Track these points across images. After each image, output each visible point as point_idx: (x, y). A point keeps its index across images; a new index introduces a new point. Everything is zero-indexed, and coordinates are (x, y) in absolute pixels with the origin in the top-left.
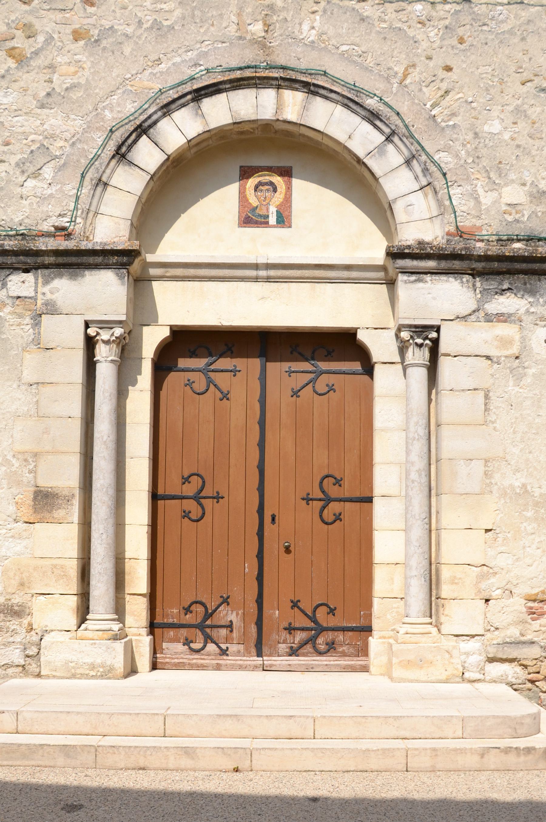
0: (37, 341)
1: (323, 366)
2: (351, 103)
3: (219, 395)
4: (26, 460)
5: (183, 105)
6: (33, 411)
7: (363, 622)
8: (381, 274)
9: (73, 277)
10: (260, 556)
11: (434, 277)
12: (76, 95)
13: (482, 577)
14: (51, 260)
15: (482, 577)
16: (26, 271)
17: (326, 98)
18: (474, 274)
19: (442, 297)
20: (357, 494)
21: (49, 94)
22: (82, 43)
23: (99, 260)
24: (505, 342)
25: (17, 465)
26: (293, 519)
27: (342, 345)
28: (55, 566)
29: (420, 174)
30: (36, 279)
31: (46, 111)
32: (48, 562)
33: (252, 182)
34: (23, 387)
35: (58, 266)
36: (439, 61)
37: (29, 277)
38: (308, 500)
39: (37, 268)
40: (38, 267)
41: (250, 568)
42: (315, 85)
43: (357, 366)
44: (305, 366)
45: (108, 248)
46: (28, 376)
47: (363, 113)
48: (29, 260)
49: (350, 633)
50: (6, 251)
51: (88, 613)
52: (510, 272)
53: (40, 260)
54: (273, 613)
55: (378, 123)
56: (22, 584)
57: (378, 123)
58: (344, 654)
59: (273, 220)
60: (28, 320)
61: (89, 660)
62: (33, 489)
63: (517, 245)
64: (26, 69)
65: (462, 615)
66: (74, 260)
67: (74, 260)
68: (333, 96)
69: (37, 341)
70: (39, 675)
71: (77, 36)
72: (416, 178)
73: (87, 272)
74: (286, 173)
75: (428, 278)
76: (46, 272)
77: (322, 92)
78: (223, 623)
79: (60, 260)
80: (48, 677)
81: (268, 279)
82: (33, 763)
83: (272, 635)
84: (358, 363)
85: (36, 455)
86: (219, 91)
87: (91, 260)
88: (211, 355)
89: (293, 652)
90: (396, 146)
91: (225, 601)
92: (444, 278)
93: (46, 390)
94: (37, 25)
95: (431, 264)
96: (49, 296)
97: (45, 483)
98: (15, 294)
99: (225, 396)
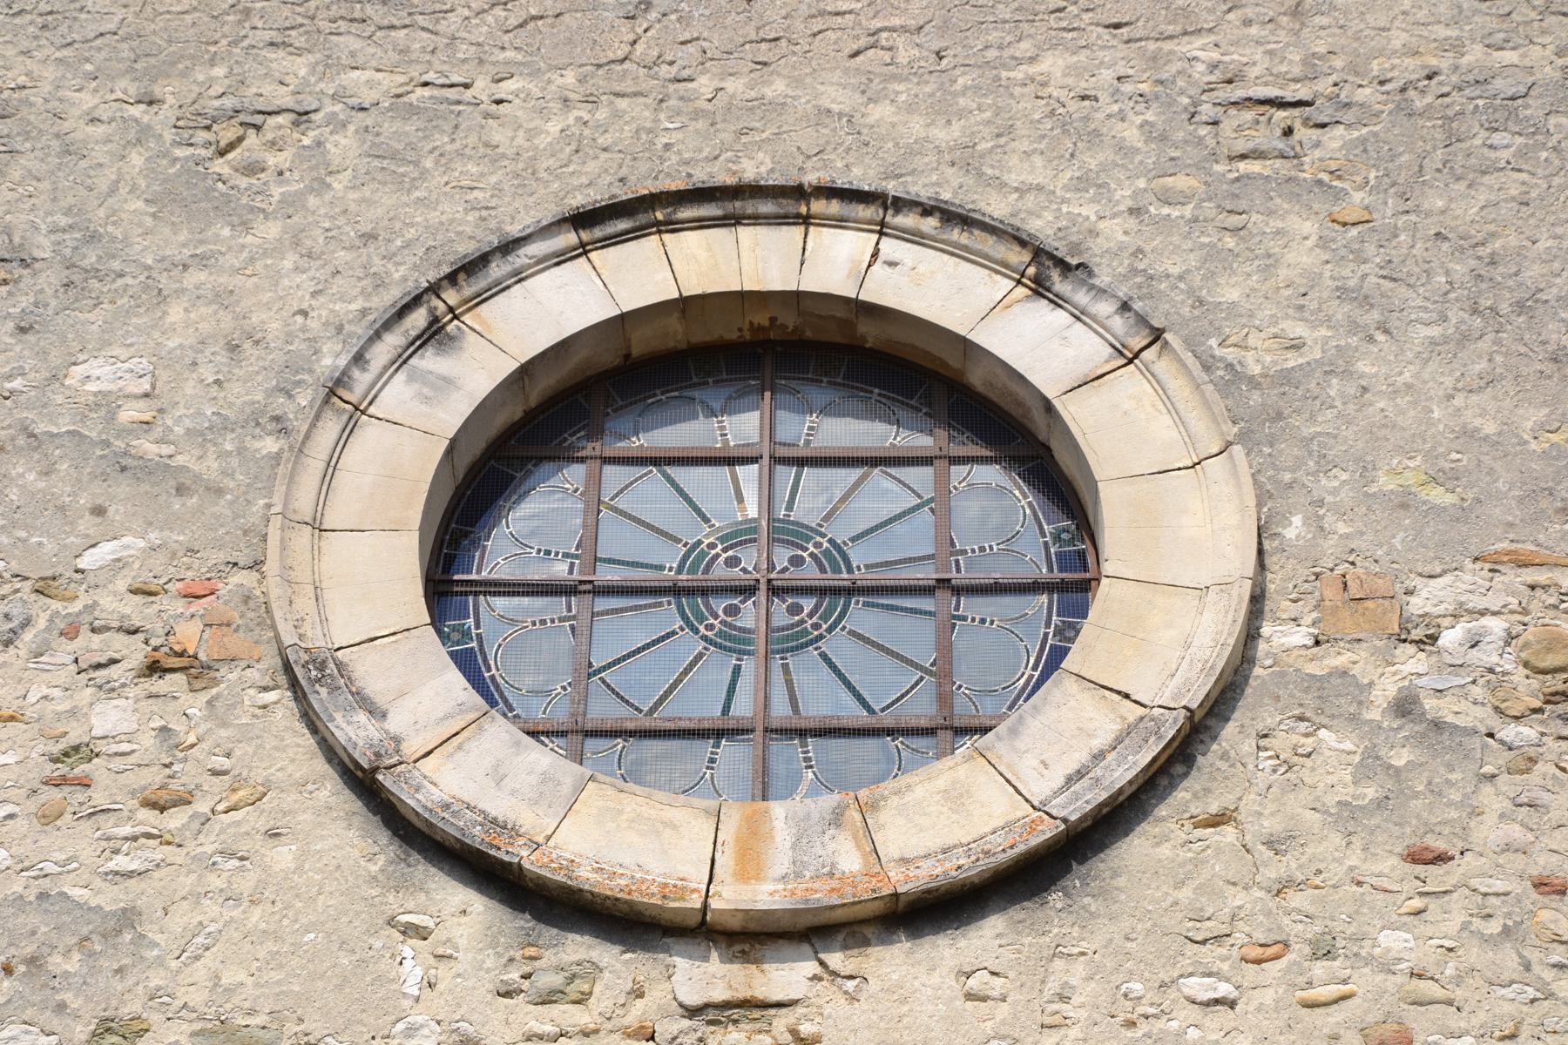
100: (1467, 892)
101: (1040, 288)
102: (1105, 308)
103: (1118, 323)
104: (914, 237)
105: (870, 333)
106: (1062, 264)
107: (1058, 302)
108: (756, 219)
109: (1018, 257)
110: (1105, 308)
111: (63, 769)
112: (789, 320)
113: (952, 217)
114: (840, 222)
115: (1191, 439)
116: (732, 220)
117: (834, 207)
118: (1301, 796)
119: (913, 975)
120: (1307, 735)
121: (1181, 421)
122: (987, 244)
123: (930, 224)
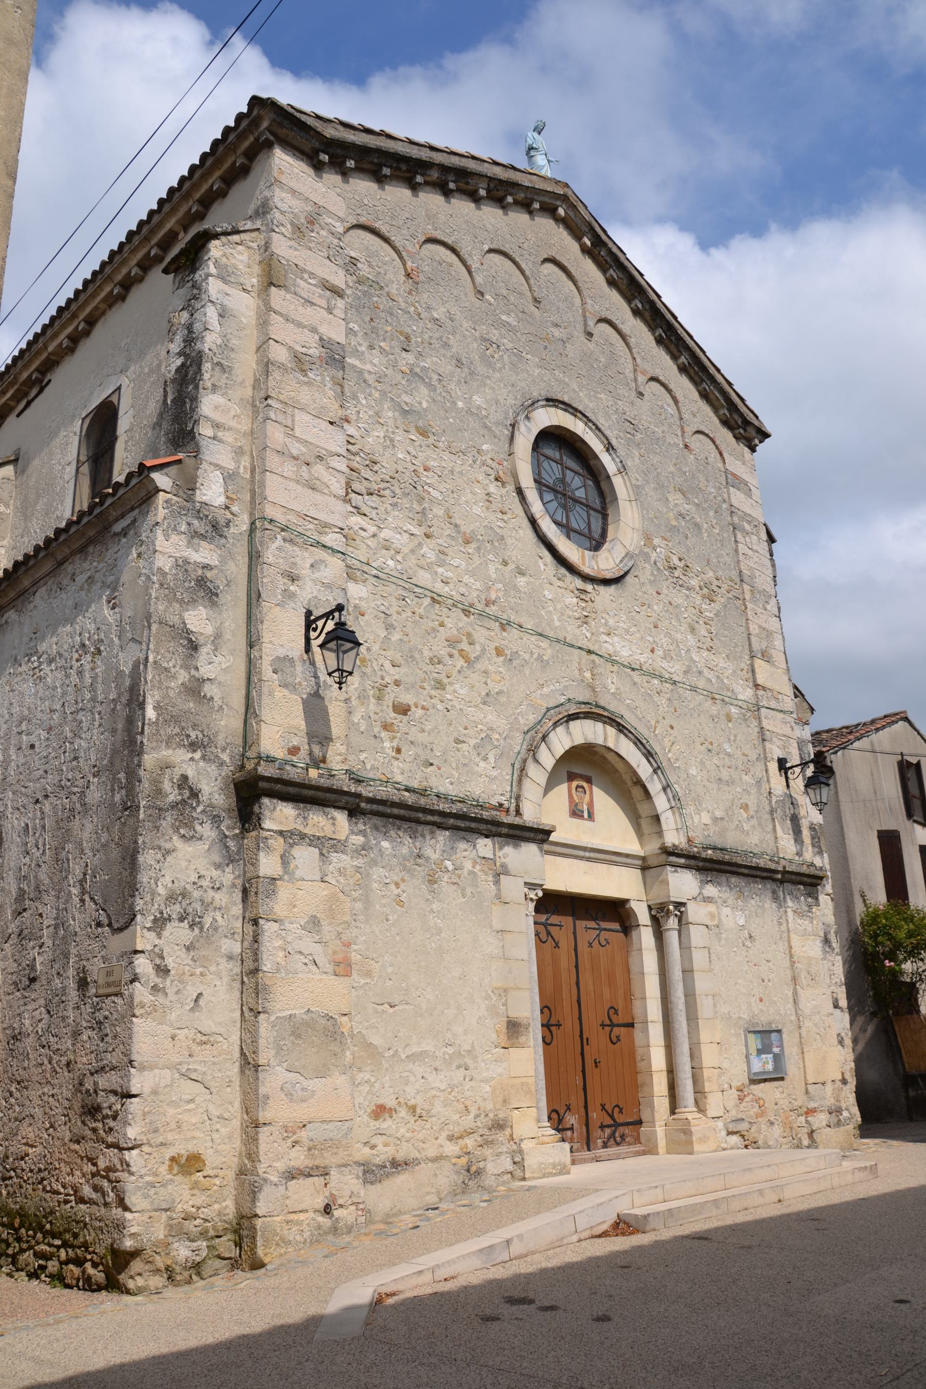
0: (498, 896)
1: (604, 925)
2: (638, 742)
3: (554, 944)
4: (500, 995)
5: (561, 724)
6: (501, 954)
7: (635, 1118)
8: (640, 862)
9: (516, 846)
10: (584, 1072)
11: (682, 870)
12: (503, 699)
13: (719, 1076)
14: (505, 830)
15: (719, 1076)
16: (487, 837)
17: (626, 736)
18: (698, 869)
19: (682, 884)
20: (625, 1021)
21: (487, 694)
22: (502, 659)
23: (532, 835)
24: (712, 915)
25: (495, 999)
26: (598, 1040)
27: (614, 911)
28: (523, 1083)
29: (671, 799)
30: (494, 845)
31: (486, 707)
32: (517, 1081)
33: (575, 784)
34: (493, 934)
35: (508, 836)
36: (667, 722)
37: (488, 841)
38: (559, 1025)
39: (494, 836)
40: (500, 835)
41: (579, 1080)
42: (623, 726)
43: (616, 926)
44: (592, 924)
45: (540, 827)
46: (497, 925)
47: (644, 750)
48: (493, 829)
49: (630, 1127)
50: (483, 819)
51: (676, 1108)
52: (712, 870)
53: (499, 829)
54: (594, 1115)
55: (651, 759)
56: (505, 1101)
57: (651, 759)
58: (629, 1144)
59: (586, 815)
60: (491, 878)
61: (551, 1161)
62: (506, 1019)
63: (710, 852)
64: (472, 670)
65: (714, 1103)
66: (518, 833)
67: (518, 833)
68: (630, 735)
69: (498, 896)
70: (524, 1179)
71: (499, 652)
72: (669, 800)
73: (522, 844)
74: (589, 780)
75: (679, 869)
76: (500, 839)
77: (625, 731)
78: (568, 1126)
79: (512, 832)
80: (530, 1179)
81: (589, 859)
82: (703, 1216)
83: (596, 1133)
84: (618, 924)
85: (505, 991)
86: (577, 718)
87: (528, 834)
88: (547, 912)
89: (605, 1145)
90: (658, 777)
91: (568, 1108)
92: (685, 870)
93: (508, 936)
94: (475, 636)
95: (682, 861)
96: (503, 860)
97: (513, 1014)
98: (482, 855)
99: (557, 946)
100: (339, 391)
101: (608, 450)
102: (618, 460)
103: (619, 464)
104: (591, 429)
105: (578, 444)
106: (613, 448)
107: (610, 454)
108: (569, 412)
109: (606, 442)
110: (618, 460)
111: (814, 881)
112: (568, 435)
113: (598, 428)
114: (580, 419)
115: (629, 495)
116: (565, 410)
117: (580, 416)
118: (217, 796)
119: (922, 732)
120: (195, 1070)
121: (627, 490)
122: (601, 436)
123: (594, 427)
